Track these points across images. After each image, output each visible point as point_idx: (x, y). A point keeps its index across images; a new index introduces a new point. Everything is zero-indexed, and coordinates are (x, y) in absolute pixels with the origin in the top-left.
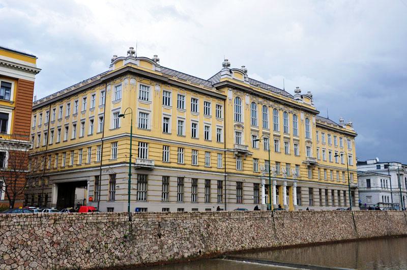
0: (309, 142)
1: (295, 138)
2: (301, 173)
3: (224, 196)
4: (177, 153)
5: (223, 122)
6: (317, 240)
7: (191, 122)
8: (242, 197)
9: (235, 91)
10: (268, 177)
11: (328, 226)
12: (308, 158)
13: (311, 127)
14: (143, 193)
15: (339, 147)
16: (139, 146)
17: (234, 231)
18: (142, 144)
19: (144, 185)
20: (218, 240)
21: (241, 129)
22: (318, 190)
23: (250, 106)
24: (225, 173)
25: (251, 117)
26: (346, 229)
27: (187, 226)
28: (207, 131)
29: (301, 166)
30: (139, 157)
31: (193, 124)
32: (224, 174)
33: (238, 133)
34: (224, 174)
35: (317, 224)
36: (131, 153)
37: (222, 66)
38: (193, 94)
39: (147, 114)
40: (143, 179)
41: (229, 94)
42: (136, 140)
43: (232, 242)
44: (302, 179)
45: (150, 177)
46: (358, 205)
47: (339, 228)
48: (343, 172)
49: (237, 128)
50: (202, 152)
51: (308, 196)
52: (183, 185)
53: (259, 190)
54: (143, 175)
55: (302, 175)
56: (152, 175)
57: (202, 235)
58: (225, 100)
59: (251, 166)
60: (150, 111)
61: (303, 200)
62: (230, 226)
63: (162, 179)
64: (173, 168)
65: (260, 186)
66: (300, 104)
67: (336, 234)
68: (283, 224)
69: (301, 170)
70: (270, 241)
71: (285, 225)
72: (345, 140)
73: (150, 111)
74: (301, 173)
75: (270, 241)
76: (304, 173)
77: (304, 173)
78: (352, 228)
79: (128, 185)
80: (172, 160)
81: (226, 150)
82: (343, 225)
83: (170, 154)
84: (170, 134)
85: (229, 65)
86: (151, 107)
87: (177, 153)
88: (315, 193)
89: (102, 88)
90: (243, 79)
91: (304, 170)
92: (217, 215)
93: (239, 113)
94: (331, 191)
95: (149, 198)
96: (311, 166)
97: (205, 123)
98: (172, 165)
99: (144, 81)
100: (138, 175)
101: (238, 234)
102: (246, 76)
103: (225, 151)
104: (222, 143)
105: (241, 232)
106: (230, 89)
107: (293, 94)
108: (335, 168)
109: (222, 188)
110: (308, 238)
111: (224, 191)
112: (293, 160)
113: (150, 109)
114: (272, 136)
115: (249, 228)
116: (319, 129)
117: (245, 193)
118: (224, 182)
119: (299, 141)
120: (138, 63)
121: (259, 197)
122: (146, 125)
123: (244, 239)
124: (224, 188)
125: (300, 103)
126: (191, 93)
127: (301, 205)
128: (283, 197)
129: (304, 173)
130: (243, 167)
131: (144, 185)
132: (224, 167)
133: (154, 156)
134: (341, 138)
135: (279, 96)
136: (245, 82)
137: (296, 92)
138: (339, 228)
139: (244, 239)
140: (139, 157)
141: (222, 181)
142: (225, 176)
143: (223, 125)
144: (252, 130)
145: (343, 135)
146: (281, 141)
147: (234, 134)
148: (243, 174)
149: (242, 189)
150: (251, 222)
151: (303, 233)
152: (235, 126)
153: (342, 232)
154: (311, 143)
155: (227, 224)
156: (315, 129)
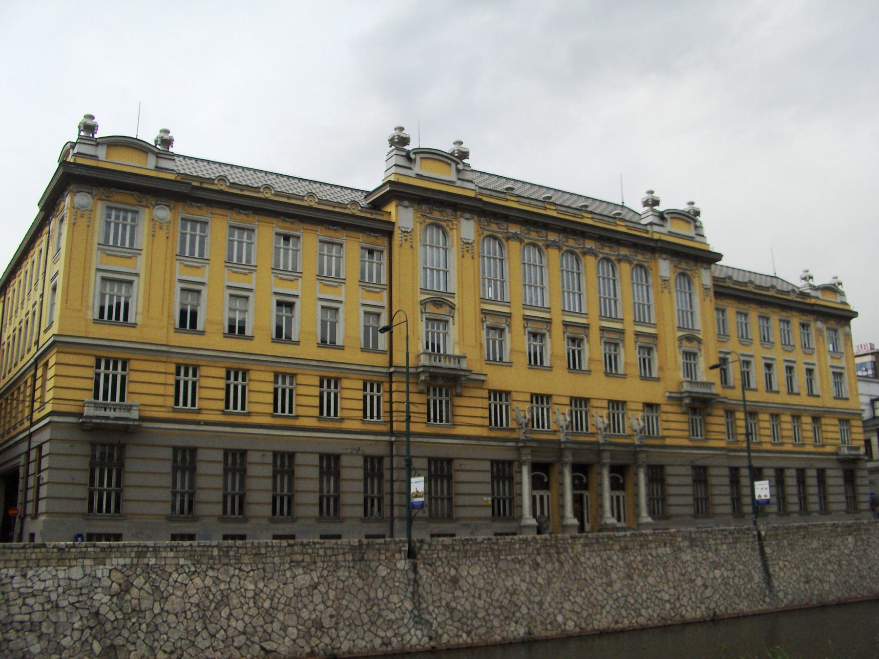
0: (690, 338)
1: (639, 329)
2: (666, 425)
3: (387, 500)
4: (485, 403)
5: (385, 294)
6: (603, 621)
7: (274, 300)
8: (450, 500)
9: (424, 207)
10: (754, 451)
11: (651, 580)
12: (685, 384)
13: (697, 299)
14: (183, 495)
15: (778, 345)
16: (490, 399)
17: (235, 601)
18: (576, 401)
19: (445, 482)
20: (163, 628)
21: (445, 310)
22: (726, 472)
23: (672, 282)
24: (391, 433)
25: (104, 217)
26: (726, 584)
27: (39, 586)
28: (745, 369)
29: (664, 408)
30: (96, 396)
31: (787, 367)
32: (387, 438)
33: (689, 355)
34: (387, 438)
35: (608, 574)
36: (408, 411)
37: (387, 144)
38: (281, 224)
39: (131, 283)
40: (505, 470)
41: (401, 216)
42: (90, 352)
43: (221, 635)
44: (668, 442)
45: (131, 451)
46: (865, 506)
47: (699, 582)
48: (793, 417)
49: (430, 308)
50: (786, 418)
51: (727, 489)
52: (245, 471)
53: (511, 478)
54: (112, 446)
55: (666, 433)
56: (137, 445)
57: (97, 614)
58: (390, 235)
59: (480, 412)
60: (137, 275)
61: (672, 500)
62: (222, 586)
63: (489, 468)
64: (207, 423)
65: (515, 467)
66: (656, 236)
67: (685, 601)
68: (455, 581)
69: (664, 417)
70: (390, 633)
71: (462, 582)
72: (819, 331)
73: (137, 275)
74: (666, 425)
75: (390, 633)
76: (673, 425)
77: (674, 427)
78: (751, 579)
79: (222, 478)
80: (346, 414)
81: (392, 370)
82: (717, 573)
83: (201, 387)
84: (202, 333)
85: (656, 203)
86: (141, 264)
87: (485, 403)
88: (830, 481)
89: (324, 233)
90: (453, 177)
91: (671, 417)
92: (172, 554)
93: (689, 309)
94: (793, 473)
95: (460, 513)
96: (698, 406)
97: (806, 363)
98: (347, 425)
99: (118, 197)
100: (93, 445)
101: (253, 611)
102: (460, 167)
103: (391, 373)
104: (383, 352)
105: (267, 604)
106: (406, 203)
107: (640, 209)
108: (786, 407)
109: (381, 476)
110: (560, 618)
111: (386, 487)
112: (635, 392)
113: (135, 268)
114: (595, 333)
115: (304, 592)
116: (724, 303)
117: (671, 490)
118: (387, 461)
119: (654, 336)
120: (101, 152)
121: (511, 500)
122: (541, 354)
123: (276, 626)
124: (387, 475)
125: (659, 233)
126: (275, 220)
127: (665, 517)
128: (601, 495)
129: (673, 425)
130: (454, 415)
131: (445, 482)
132: (388, 419)
133: (149, 392)
134: (804, 326)
135: (583, 217)
136: (459, 183)
137: (646, 204)
138: (699, 582)
139: (276, 626)
140: (96, 396)
141: (380, 459)
142: (391, 443)
143: (385, 303)
144: (484, 312)
145: (811, 318)
146: (591, 335)
147: (681, 360)
148: (198, 423)
149: (705, 482)
150: (315, 575)
151: (540, 604)
152: (680, 339)
153: (708, 592)
154: (699, 341)
155: (209, 582)
156: (710, 304)
